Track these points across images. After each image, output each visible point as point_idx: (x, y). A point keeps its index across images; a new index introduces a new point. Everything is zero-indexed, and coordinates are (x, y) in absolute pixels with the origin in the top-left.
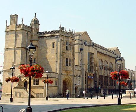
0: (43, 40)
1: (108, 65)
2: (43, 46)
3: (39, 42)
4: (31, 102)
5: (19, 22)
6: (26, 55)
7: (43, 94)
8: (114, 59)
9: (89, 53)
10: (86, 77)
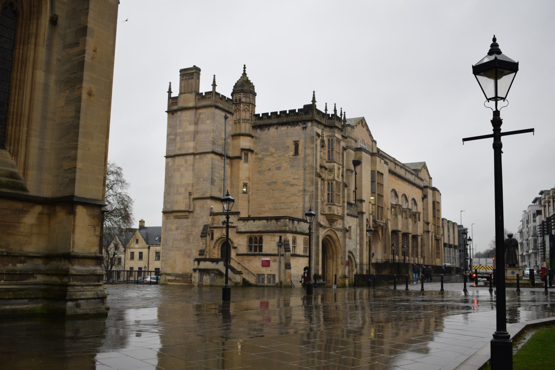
0: (266, 134)
2: (267, 150)
3: (254, 138)
4: (496, 316)
5: (205, 87)
6: (222, 172)
7: (274, 276)
9: (374, 171)
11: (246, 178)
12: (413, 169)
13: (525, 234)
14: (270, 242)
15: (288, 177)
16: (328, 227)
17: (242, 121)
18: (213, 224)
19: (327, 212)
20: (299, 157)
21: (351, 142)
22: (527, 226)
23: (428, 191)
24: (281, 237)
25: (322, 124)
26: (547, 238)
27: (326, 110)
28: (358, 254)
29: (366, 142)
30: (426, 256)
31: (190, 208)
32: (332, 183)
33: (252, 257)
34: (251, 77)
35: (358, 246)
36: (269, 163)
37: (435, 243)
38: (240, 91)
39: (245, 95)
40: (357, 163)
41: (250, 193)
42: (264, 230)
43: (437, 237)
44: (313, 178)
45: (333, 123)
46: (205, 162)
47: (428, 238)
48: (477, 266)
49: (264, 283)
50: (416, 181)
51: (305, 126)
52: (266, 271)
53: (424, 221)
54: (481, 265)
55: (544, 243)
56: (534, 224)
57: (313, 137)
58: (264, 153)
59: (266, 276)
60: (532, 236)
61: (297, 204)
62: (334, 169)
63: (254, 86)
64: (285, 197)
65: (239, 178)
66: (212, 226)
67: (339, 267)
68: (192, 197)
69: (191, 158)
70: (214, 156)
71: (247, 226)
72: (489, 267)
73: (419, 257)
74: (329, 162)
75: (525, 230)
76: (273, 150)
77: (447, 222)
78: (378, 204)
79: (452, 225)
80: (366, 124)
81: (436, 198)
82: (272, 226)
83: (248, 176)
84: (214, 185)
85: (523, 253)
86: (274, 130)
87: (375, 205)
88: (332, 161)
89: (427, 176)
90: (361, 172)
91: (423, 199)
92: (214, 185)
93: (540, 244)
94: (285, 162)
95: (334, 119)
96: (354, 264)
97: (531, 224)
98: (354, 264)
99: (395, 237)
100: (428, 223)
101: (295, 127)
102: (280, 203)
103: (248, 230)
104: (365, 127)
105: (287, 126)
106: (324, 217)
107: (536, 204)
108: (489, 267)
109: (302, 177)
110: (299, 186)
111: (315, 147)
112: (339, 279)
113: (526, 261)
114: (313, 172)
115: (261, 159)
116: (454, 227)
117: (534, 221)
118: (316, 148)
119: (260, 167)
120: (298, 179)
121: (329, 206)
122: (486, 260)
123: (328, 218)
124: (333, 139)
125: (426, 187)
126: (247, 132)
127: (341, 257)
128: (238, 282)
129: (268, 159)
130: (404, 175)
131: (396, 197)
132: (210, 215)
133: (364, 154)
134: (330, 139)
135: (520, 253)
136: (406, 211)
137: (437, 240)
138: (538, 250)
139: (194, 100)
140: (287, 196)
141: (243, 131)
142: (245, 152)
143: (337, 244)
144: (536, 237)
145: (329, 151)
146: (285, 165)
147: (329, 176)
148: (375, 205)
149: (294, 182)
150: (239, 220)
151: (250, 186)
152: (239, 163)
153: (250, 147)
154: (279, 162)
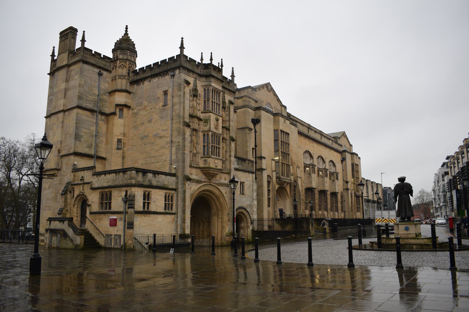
1: (325, 166)
3: (132, 94)
7: (120, 236)
8: (339, 155)
9: (277, 130)
10: (269, 199)
11: (121, 133)
12: (333, 136)
13: (437, 191)
14: (117, 198)
15: (158, 129)
16: (205, 182)
17: (117, 77)
18: (74, 180)
19: (202, 165)
20: (168, 107)
21: (250, 102)
22: (438, 185)
23: (346, 154)
24: (127, 192)
25: (194, 72)
26: (454, 192)
27: (202, 59)
28: (255, 209)
29: (272, 105)
30: (346, 210)
31: (58, 166)
32: (208, 134)
33: (103, 215)
34: (132, 36)
35: (255, 202)
36: (142, 116)
37: (355, 199)
38: (118, 48)
39: (122, 52)
40: (256, 121)
41: (125, 149)
42: (113, 184)
43: (356, 194)
44: (180, 127)
45: (209, 73)
46: (72, 117)
47: (348, 195)
48: (379, 219)
49: (111, 245)
50: (309, 134)
51: (172, 73)
52: (113, 231)
53: (344, 180)
54: (383, 218)
55: (451, 197)
56: (443, 183)
57: (180, 84)
58: (139, 108)
59: (113, 236)
60: (442, 192)
61: (165, 157)
62: (210, 119)
63: (135, 44)
64: (154, 150)
65: (113, 134)
66: (73, 183)
67: (224, 224)
68: (61, 154)
69: (61, 115)
70: (80, 111)
71: (99, 182)
72: (391, 219)
73: (340, 211)
74: (204, 113)
75: (437, 188)
76: (146, 103)
77: (371, 183)
78: (212, 143)
79: (376, 185)
80: (272, 89)
81: (354, 161)
82: (121, 179)
83: (122, 132)
84: (80, 141)
85: (436, 206)
86: (148, 83)
87: (354, 184)
88: (207, 111)
89: (348, 143)
90: (261, 129)
91: (342, 161)
92: (80, 141)
93: (449, 197)
94: (156, 114)
95: (210, 69)
96: (249, 220)
97: (441, 183)
98: (249, 220)
99: (310, 194)
100: (347, 182)
101: (165, 78)
102: (150, 157)
103: (100, 185)
104: (271, 92)
105: (158, 77)
106: (199, 170)
107: (444, 168)
108: (391, 219)
109: (170, 127)
110: (167, 137)
111: (182, 95)
112: (225, 237)
113: (439, 212)
114: (180, 121)
115: (136, 114)
116: (377, 187)
117: (443, 180)
118: (184, 96)
119: (135, 122)
120: (166, 130)
121: (205, 159)
122: (389, 213)
123: (204, 172)
124: (209, 89)
125: (345, 151)
126: (124, 88)
127: (227, 213)
128: (78, 244)
129: (143, 113)
130: (320, 139)
131: (311, 158)
132: (73, 172)
133: (263, 113)
134: (206, 89)
135: (434, 206)
136: (323, 171)
137: (357, 197)
138: (448, 203)
139: (67, 58)
140: (156, 149)
141: (119, 88)
142: (120, 108)
143: (222, 200)
144: (445, 193)
145: (205, 102)
146: (156, 117)
147: (204, 127)
148: (354, 184)
149: (163, 134)
150: (93, 175)
151: (125, 142)
152: (114, 119)
153: (126, 102)
154: (151, 115)
